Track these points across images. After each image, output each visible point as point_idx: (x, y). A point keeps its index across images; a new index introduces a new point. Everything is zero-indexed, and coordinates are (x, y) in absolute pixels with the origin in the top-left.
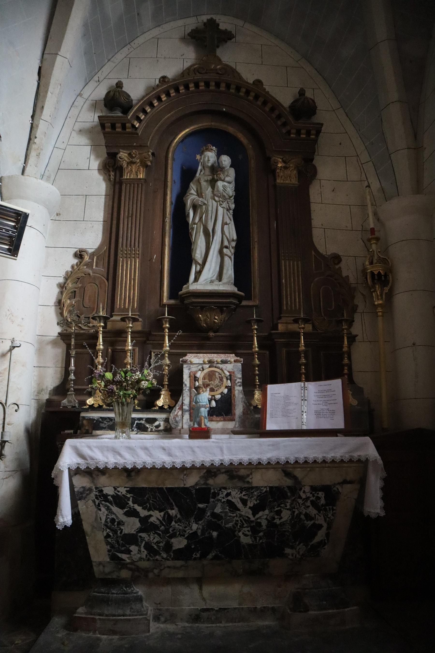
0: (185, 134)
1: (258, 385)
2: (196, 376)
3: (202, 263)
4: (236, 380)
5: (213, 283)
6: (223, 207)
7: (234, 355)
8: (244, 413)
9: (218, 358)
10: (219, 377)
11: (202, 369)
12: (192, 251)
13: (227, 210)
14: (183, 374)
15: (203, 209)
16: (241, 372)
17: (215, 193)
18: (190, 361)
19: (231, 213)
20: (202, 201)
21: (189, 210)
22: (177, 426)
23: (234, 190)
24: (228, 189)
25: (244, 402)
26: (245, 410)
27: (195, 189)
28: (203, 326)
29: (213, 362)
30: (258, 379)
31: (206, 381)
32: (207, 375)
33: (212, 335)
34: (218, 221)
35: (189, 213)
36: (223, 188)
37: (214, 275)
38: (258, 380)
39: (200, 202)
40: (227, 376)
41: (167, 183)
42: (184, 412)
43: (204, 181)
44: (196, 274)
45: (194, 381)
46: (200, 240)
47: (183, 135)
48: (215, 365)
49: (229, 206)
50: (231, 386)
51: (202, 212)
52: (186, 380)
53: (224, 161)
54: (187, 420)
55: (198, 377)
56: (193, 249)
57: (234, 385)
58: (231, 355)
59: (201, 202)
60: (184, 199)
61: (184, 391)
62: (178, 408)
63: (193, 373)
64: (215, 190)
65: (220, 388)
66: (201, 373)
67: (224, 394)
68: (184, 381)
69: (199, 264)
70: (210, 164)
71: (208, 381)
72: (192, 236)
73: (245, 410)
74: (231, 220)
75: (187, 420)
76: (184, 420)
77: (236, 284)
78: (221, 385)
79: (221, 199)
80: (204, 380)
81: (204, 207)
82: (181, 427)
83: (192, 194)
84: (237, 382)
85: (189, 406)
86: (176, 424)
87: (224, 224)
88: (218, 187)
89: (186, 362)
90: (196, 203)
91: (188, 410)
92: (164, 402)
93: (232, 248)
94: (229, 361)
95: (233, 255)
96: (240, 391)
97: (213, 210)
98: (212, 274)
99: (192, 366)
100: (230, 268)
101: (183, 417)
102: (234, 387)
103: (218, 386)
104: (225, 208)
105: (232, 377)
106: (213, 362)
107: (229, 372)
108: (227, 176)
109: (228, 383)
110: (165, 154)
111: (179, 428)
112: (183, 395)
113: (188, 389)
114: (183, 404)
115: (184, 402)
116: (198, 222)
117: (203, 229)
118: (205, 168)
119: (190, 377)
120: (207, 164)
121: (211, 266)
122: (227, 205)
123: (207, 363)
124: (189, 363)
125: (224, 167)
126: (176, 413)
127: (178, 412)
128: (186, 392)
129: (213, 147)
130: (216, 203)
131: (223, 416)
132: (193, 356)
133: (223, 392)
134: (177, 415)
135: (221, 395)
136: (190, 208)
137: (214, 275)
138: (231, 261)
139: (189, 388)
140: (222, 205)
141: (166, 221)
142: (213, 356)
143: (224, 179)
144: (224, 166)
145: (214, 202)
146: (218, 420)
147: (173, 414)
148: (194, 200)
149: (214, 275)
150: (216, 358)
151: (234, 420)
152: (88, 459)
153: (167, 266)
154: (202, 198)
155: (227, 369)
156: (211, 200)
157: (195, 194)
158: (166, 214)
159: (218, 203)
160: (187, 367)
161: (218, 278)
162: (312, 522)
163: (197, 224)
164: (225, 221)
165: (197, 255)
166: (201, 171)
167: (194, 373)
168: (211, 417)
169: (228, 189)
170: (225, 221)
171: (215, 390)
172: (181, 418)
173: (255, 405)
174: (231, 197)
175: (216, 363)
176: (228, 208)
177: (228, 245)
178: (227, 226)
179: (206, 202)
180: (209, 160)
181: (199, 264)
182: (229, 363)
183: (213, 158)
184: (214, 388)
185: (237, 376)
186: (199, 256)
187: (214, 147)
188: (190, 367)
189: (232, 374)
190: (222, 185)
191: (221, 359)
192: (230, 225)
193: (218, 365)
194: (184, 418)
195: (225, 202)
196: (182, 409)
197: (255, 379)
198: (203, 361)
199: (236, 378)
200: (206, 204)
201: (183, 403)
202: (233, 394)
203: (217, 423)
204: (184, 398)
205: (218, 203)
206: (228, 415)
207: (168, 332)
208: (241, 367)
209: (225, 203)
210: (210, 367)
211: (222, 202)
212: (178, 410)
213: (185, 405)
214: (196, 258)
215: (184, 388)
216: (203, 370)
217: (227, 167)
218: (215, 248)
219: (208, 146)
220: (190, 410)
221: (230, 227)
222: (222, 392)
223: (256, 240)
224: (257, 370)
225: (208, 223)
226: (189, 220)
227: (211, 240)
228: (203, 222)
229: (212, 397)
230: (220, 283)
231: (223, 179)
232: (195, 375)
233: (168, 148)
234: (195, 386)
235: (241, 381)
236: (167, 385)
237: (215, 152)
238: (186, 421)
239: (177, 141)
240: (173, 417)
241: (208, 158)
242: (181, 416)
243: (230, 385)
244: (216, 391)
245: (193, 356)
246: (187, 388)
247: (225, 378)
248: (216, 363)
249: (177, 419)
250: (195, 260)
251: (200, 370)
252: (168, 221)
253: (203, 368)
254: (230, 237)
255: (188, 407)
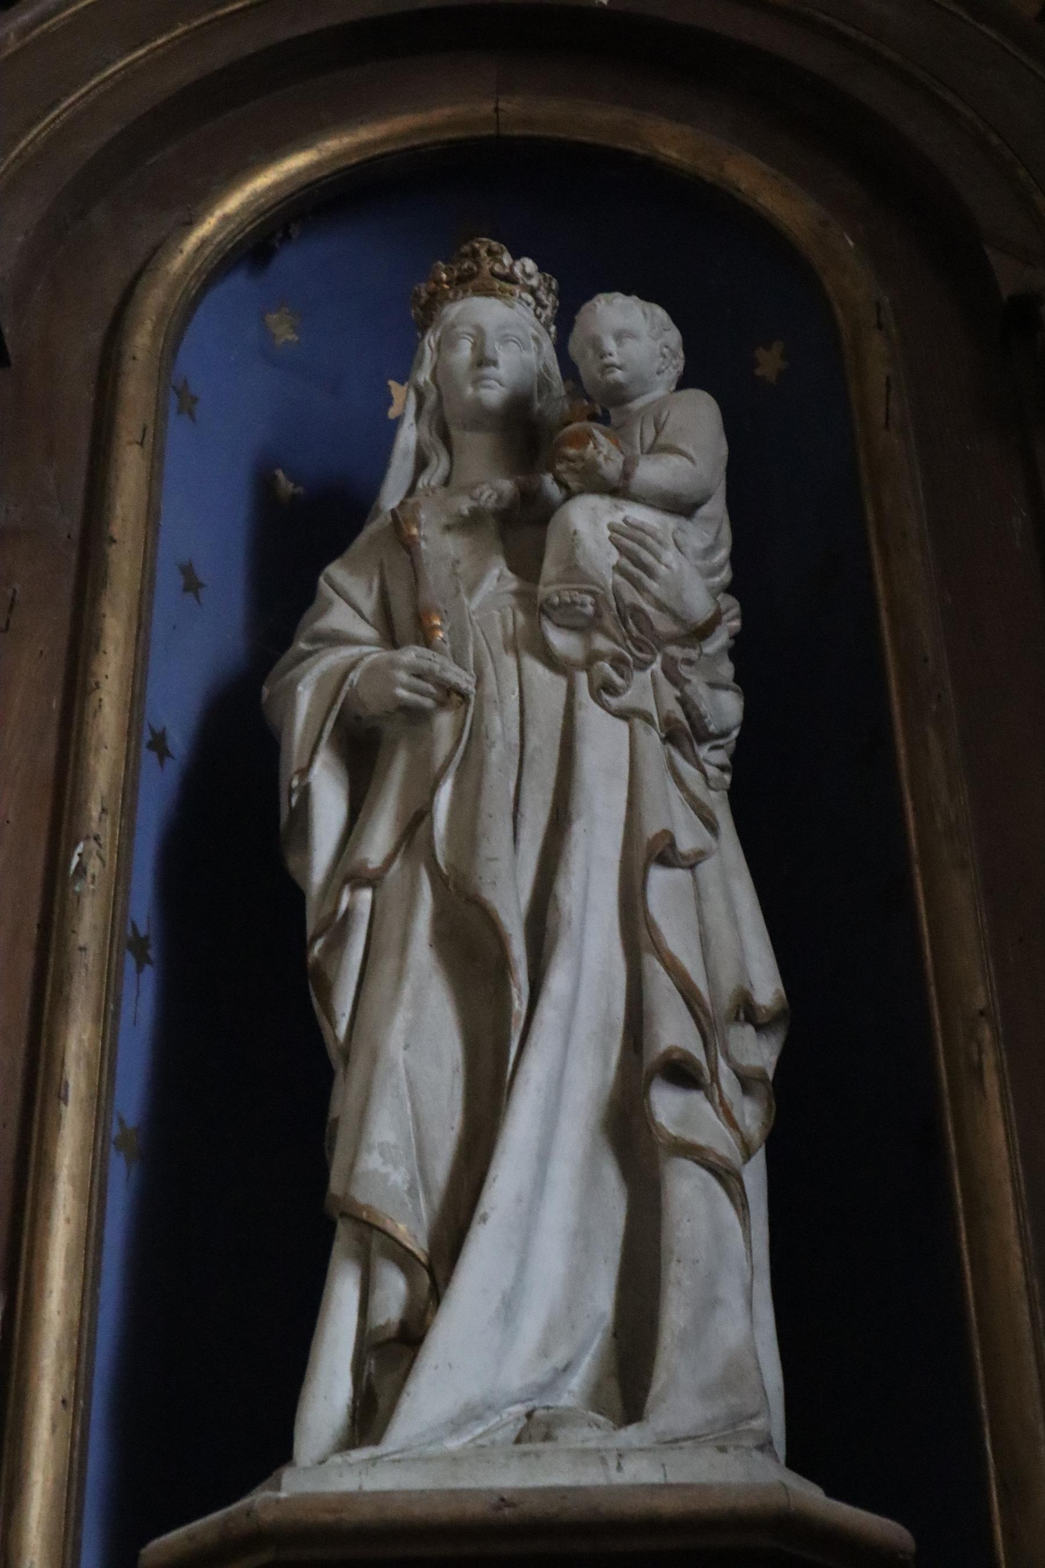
0: (275, 186)
3: (435, 1242)
5: (547, 1437)
6: (623, 714)
8: (311, 1001)
12: (332, 1149)
13: (671, 736)
15: (432, 743)
17: (548, 589)
19: (711, 771)
20: (425, 664)
21: (305, 772)
23: (725, 576)
24: (670, 555)
27: (369, 604)
34: (578, 829)
35: (302, 814)
36: (622, 550)
37: (567, 1368)
39: (403, 676)
41: (105, 556)
43: (448, 528)
44: (371, 1365)
46: (401, 1019)
47: (257, 196)
49: (684, 702)
51: (427, 758)
53: (620, 336)
56: (336, 1121)
59: (419, 675)
60: (266, 691)
64: (550, 569)
69: (404, 1258)
70: (494, 395)
72: (326, 991)
74: (711, 826)
77: (796, 1461)
79: (601, 643)
81: (444, 722)
83: (337, 639)
87: (640, 857)
88: (572, 539)
90: (372, 703)
93: (747, 1082)
95: (759, 1159)
97: (533, 741)
98: (544, 1352)
100: (731, 1291)
104: (647, 718)
106: (626, 479)
108: (656, 449)
110: (95, 337)
116: (389, 861)
117: (439, 917)
118: (454, 432)
120: (470, 391)
121: (522, 1265)
122: (669, 693)
125: (618, 386)
129: (516, 257)
130: (562, 682)
136: (314, 752)
137: (567, 1368)
138: (742, 1206)
140: (610, 688)
141: (81, 869)
143: (626, 475)
144: (619, 375)
145: (536, 670)
148: (354, 676)
149: (559, 1358)
153: (67, 1293)
154: (425, 638)
156: (509, 662)
157: (366, 631)
158: (78, 807)
159: (582, 678)
161: (613, 1387)
163: (373, 880)
164: (652, 827)
165: (372, 1162)
166: (421, 464)
169: (670, 555)
170: (652, 827)
174: (703, 632)
176: (680, 715)
177: (699, 1055)
178: (680, 875)
179: (463, 680)
180: (482, 361)
181: (404, 1258)
183: (523, 346)
186: (399, 1177)
187: (530, 265)
190: (612, 528)
192: (708, 869)
195: (643, 665)
200: (464, 696)
205: (582, 678)
209: (642, 678)
211: (618, 662)
214: (364, 1195)
217: (644, 384)
218: (558, 1082)
219: (475, 253)
221: (713, 891)
223: (980, 998)
225: (486, 849)
226: (307, 866)
227: (519, 1005)
228: (433, 855)
230: (631, 1434)
231: (611, 468)
233: (128, 296)
237: (539, 303)
239: (204, 242)
241: (479, 346)
250: (358, 1221)
252: (94, 866)
254: (710, 979)
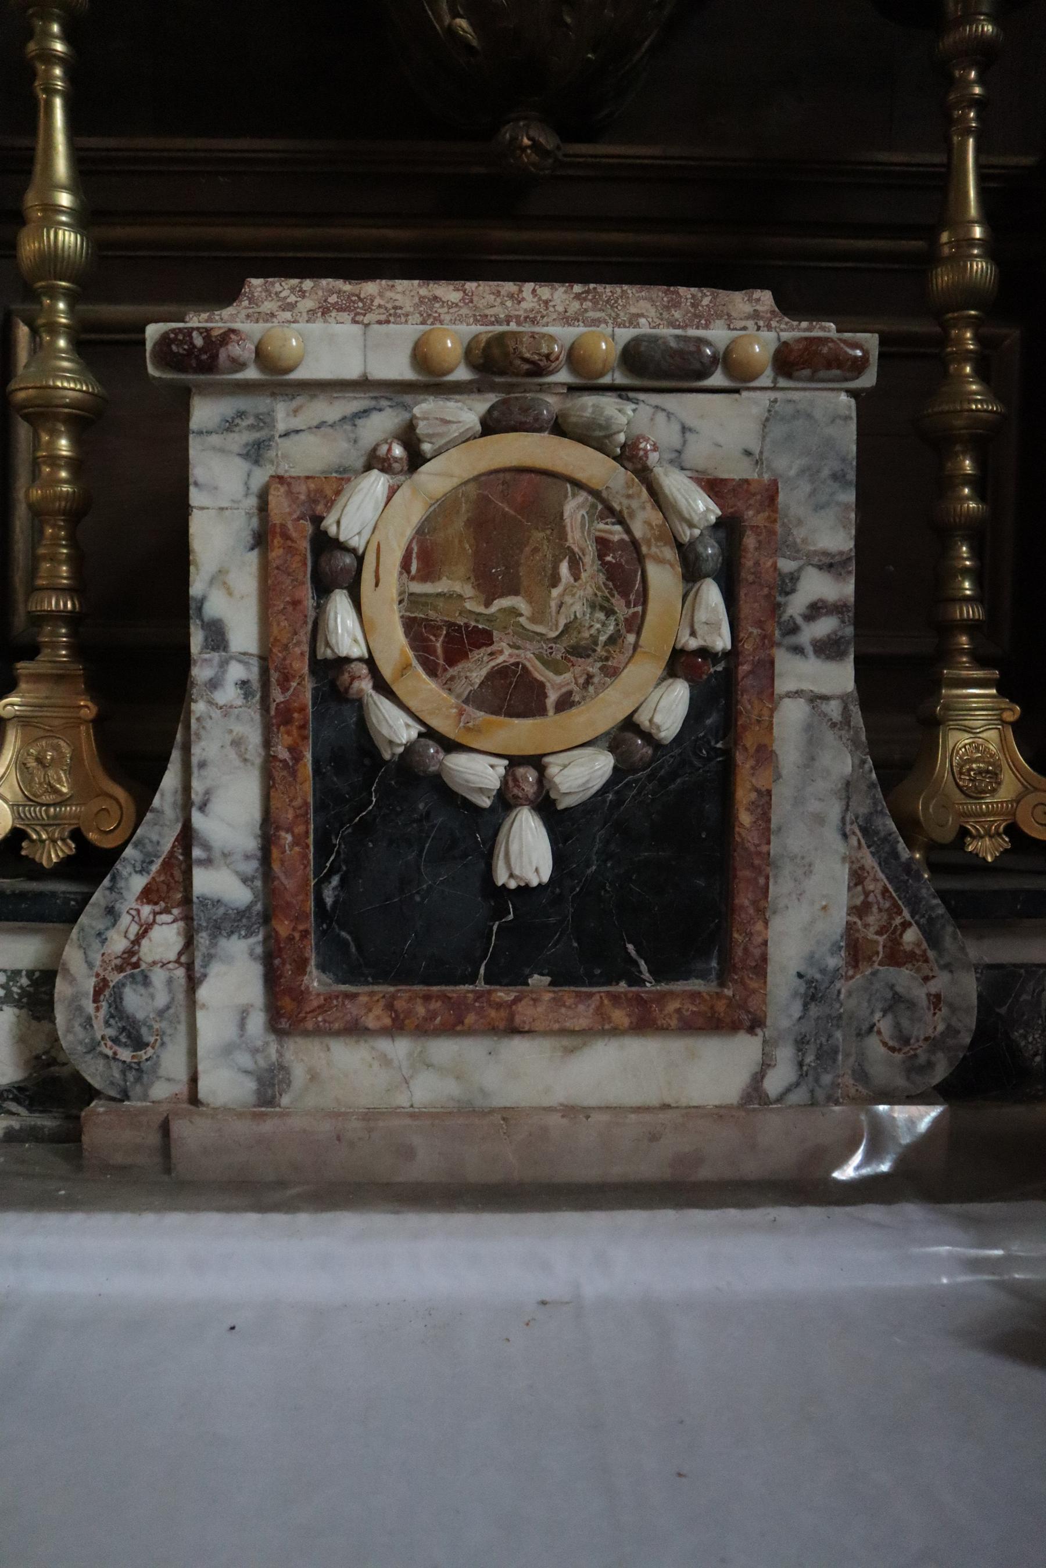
1: (971, 627)
2: (330, 525)
4: (788, 584)
7: (765, 298)
9: (595, 322)
10: (603, 545)
11: (398, 451)
14: (182, 510)
16: (849, 497)
18: (261, 356)
22: (138, 1071)
25: (865, 831)
26: (874, 919)
28: (451, 31)
29: (538, 369)
30: (978, 576)
31: (442, 586)
32: (459, 524)
33: (536, 146)
38: (979, 582)
40: (686, 534)
42: (203, 939)
45: (307, 595)
48: (552, 403)
50: (732, 655)
52: (219, 577)
54: (242, 1025)
55: (357, 543)
57: (767, 642)
58: (739, 302)
61: (199, 707)
62: (138, 883)
63: (302, 490)
65: (612, 673)
66: (392, 492)
67: (648, 737)
68: (196, 588)
71: (467, 590)
73: (874, 919)
75: (242, 1025)
76: (202, 1020)
78: (612, 640)
80: (428, 574)
82: (181, 1088)
84: (796, 605)
85: (251, 867)
86: (125, 1054)
89: (210, 366)
91: (242, 914)
92: (31, 800)
94: (726, 360)
96: (834, 709)
99: (283, 416)
101: (193, 983)
102: (767, 668)
103: (580, 651)
105: (750, 541)
106: (538, 369)
107: (713, 487)
109: (701, 616)
111: (160, 1091)
112: (187, 749)
113: (244, 684)
114: (197, 853)
115: (198, 820)
119: (261, 539)
123: (462, 374)
124: (252, 373)
126: (118, 944)
127: (145, 930)
128: (226, 710)
131: (636, 980)
132: (308, 304)
133: (643, 719)
134: (130, 960)
135: (612, 749)
139: (253, 674)
142: (529, 302)
146: (582, 1023)
147: (85, 949)
150: (567, 320)
151: (755, 1025)
152: (402, 597)
155: (698, 452)
160: (229, 426)
162: (608, 582)
167: (313, 501)
168: (504, 995)
171: (552, 697)
172: (181, 997)
173: (946, 835)
175: (563, 376)
182: (717, 379)
184: (540, 673)
185: (799, 534)
188: (264, 421)
189: (753, 517)
191: (625, 334)
193: (589, 402)
194: (203, 993)
196: (187, 900)
197: (950, 574)
198: (420, 357)
199: (786, 565)
201: (187, 836)
202: (749, 741)
203: (570, 1051)
204: (198, 786)
206: (686, 976)
207: (62, 61)
208: (847, 438)
210: (489, 427)
212: (146, 910)
213: (208, 862)
215: (200, 673)
216: (416, 460)
220: (266, 918)
222: (629, 724)
224: (968, 480)
229: (509, 779)
232: (317, 520)
234: (322, 652)
235: (845, 590)
236: (71, 619)
238: (230, 1032)
240: (89, 985)
242: (180, 973)
243: (722, 641)
244: (565, 703)
245: (308, 304)
246: (236, 672)
247: (669, 553)
248: (563, 376)
249: (134, 1000)
251: (375, 461)
253: (409, 437)
255: (246, 880)
